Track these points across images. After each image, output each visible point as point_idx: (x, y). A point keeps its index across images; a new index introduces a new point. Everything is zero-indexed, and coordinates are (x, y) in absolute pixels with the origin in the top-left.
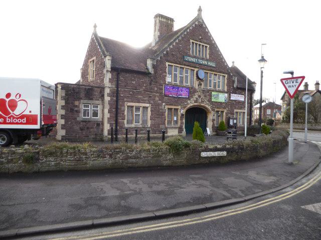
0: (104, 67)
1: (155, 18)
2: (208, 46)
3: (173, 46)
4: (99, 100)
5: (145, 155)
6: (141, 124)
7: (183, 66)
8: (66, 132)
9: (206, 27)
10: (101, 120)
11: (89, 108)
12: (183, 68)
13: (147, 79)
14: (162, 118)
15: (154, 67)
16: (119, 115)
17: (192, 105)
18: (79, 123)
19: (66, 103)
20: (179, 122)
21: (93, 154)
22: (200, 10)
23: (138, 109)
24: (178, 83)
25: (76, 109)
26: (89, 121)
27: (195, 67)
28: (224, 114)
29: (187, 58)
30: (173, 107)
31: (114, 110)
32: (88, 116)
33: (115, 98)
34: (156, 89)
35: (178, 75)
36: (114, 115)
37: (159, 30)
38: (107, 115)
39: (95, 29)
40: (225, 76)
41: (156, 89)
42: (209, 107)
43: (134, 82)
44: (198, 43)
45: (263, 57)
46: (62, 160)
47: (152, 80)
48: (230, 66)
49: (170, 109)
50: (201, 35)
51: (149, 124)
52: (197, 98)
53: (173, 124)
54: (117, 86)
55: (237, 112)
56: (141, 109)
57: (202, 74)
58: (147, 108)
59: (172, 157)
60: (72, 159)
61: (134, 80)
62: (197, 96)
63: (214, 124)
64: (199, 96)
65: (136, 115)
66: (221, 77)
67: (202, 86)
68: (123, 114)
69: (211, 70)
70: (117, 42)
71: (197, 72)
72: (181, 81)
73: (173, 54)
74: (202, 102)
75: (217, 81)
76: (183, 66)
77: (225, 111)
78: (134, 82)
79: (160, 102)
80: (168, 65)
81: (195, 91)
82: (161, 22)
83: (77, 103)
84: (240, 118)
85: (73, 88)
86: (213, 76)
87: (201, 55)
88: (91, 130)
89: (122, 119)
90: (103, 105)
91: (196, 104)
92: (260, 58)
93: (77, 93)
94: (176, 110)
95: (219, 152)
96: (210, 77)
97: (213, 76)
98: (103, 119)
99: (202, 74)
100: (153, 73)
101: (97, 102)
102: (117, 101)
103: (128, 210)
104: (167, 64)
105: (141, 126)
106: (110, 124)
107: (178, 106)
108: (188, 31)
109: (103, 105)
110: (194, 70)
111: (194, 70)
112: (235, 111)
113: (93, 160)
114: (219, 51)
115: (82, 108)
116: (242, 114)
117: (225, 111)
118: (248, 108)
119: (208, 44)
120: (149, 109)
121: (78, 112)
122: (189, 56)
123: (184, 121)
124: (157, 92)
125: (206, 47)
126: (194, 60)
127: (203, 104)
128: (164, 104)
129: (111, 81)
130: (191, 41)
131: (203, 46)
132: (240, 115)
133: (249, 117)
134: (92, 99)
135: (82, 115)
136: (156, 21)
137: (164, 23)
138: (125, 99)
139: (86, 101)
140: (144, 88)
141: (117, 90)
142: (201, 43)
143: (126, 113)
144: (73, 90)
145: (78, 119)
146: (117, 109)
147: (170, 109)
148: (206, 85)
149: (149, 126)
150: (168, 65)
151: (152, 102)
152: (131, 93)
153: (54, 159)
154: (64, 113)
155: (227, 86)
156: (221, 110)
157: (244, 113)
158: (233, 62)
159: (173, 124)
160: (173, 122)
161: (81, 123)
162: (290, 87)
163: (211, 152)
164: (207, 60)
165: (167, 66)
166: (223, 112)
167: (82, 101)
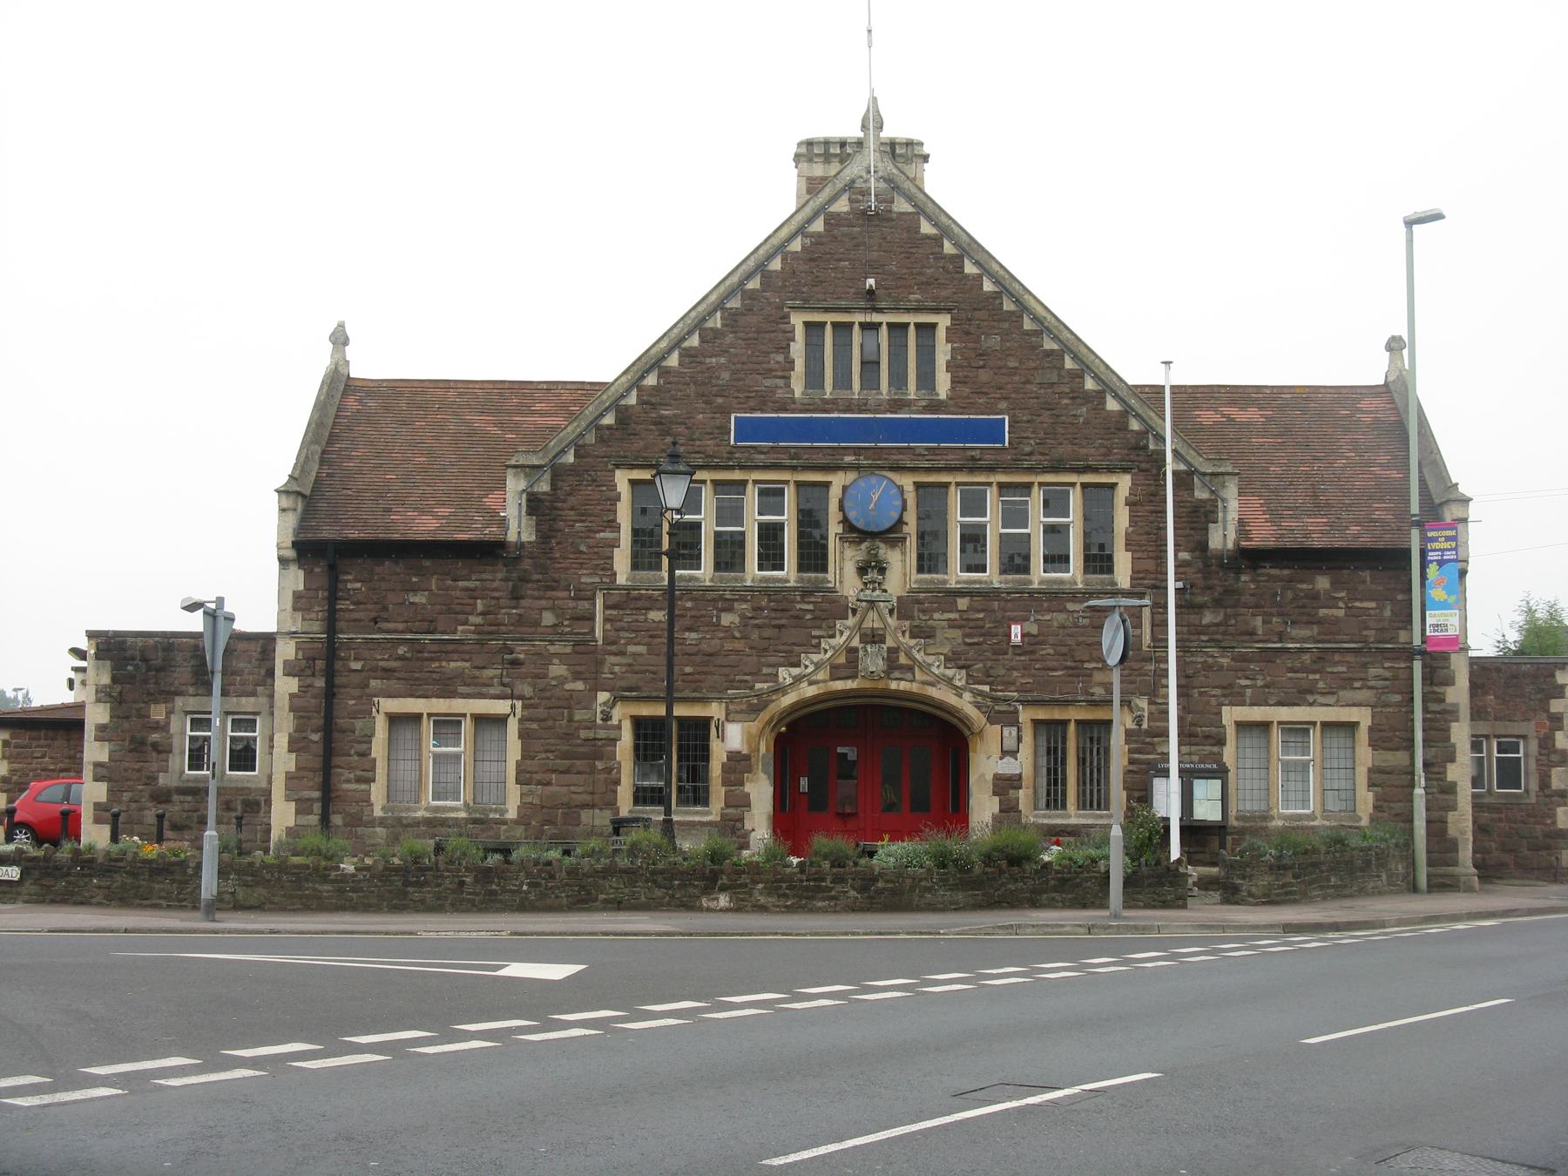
4: (254, 694)
7: (737, 475)
10: (264, 784)
13: (495, 577)
14: (592, 770)
15: (534, 504)
16: (336, 760)
17: (809, 691)
18: (162, 797)
23: (447, 725)
28: (1117, 741)
31: (316, 737)
33: (320, 683)
36: (317, 763)
41: (548, 619)
42: (965, 704)
43: (419, 599)
50: (874, 268)
54: (331, 627)
58: (501, 721)
61: (415, 590)
65: (437, 757)
68: (365, 754)
70: (123, 911)
73: (658, 422)
79: (580, 685)
83: (157, 712)
85: (142, 651)
89: (359, 780)
91: (839, 685)
93: (158, 670)
98: (270, 778)
100: (529, 536)
102: (330, 694)
103: (1049, 404)
104: (622, 479)
105: (463, 815)
107: (704, 700)
110: (933, 326)
111: (933, 326)
112: (1231, 715)
115: (183, 732)
119: (937, 310)
120: (513, 726)
121: (163, 750)
125: (927, 330)
127: (903, 686)
131: (898, 329)
140: (479, 620)
144: (144, 660)
146: (328, 729)
148: (929, 560)
149: (512, 814)
150: (633, 483)
154: (103, 798)
161: (175, 798)
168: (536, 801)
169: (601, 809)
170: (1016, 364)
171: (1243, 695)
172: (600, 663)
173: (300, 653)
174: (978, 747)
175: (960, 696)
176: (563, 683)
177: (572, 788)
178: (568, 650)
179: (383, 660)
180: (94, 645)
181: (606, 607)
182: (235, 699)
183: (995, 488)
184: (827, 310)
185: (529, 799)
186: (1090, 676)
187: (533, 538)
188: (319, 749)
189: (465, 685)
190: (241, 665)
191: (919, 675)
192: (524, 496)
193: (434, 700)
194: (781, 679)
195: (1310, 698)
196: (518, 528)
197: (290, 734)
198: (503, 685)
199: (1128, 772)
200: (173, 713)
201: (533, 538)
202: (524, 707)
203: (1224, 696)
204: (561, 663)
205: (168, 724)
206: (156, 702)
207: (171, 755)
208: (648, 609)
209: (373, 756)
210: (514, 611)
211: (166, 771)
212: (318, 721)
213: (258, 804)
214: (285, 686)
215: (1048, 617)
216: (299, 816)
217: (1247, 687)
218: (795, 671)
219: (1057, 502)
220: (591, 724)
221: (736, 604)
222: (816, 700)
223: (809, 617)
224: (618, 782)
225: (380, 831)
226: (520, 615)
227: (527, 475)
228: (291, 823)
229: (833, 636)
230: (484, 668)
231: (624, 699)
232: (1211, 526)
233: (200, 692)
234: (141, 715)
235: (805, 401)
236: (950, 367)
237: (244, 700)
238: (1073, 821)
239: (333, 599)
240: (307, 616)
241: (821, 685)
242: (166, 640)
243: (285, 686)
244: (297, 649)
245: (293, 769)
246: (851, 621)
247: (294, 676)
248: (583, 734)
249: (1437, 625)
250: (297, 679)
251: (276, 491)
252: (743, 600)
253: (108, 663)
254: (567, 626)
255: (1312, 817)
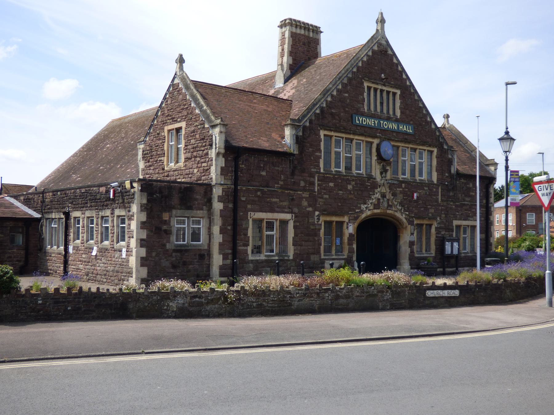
0: (211, 145)
1: (281, 27)
2: (398, 92)
3: (332, 96)
4: (202, 209)
5: (358, 294)
6: (277, 254)
8: (148, 273)
9: (394, 54)
10: (206, 247)
11: (186, 226)
12: (352, 140)
15: (298, 140)
16: (238, 237)
17: (369, 213)
19: (149, 216)
20: (346, 247)
21: (298, 293)
22: (382, 21)
23: (270, 225)
24: (342, 169)
25: (165, 227)
26: (187, 251)
27: (375, 137)
28: (433, 230)
29: (360, 120)
30: (335, 219)
31: (229, 228)
32: (184, 241)
33: (231, 206)
34: (302, 184)
35: (343, 156)
37: (291, 53)
38: (218, 238)
39: (181, 68)
40: (432, 152)
41: (302, 184)
42: (402, 217)
43: (264, 173)
44: (380, 87)
45: (507, 133)
46: (264, 300)
47: (295, 168)
48: (439, 125)
49: (328, 224)
50: (382, 71)
51: (291, 253)
52: (379, 199)
53: (333, 252)
54: (236, 184)
55: (458, 227)
56: (276, 225)
57: (387, 149)
59: (390, 296)
60: (275, 299)
62: (378, 196)
63: (412, 252)
64: (383, 196)
66: (425, 155)
67: (389, 175)
69: (406, 141)
71: (378, 146)
72: (348, 168)
73: (332, 114)
74: (390, 207)
75: (416, 163)
76: (351, 136)
77: (435, 225)
78: (264, 173)
79: (310, 209)
80: (325, 135)
81: (375, 185)
82: (293, 35)
83: (166, 216)
84: (465, 239)
86: (408, 152)
87: (385, 111)
88: (191, 266)
90: (210, 218)
92: (502, 134)
94: (340, 224)
95: (450, 291)
96: (404, 155)
97: (408, 152)
98: (209, 245)
99: (387, 149)
101: (200, 213)
102: (235, 210)
104: (322, 133)
105: (277, 258)
106: (223, 254)
107: (342, 215)
108: (360, 64)
109: (210, 218)
112: (456, 223)
113: (299, 301)
114: (420, 100)
116: (469, 231)
117: (435, 225)
118: (481, 217)
119: (397, 88)
120: (291, 225)
121: (168, 233)
122: (363, 114)
123: (355, 246)
124: (304, 190)
125: (394, 94)
126: (371, 122)
128: (317, 213)
129: (224, 171)
130: (366, 84)
131: (388, 92)
132: (465, 232)
133: (484, 236)
134: (190, 208)
135: (173, 238)
136: (283, 35)
137: (322, 32)
138: (249, 206)
139: (179, 212)
140: (281, 183)
141: (236, 191)
142: (384, 88)
143: (250, 233)
145: (168, 246)
147: (328, 224)
148: (395, 172)
149: (291, 258)
150: (325, 135)
151: (296, 210)
152: (259, 193)
153: (256, 299)
155: (437, 171)
156: (425, 222)
157: (474, 227)
158: (447, 117)
159: (333, 252)
160: (334, 248)
161: (174, 254)
162: (543, 195)
163: (439, 291)
164: (397, 121)
165: (322, 137)
166: (430, 226)
167: (174, 212)
168: (299, 252)
169: (316, 255)
170: (414, 110)
171: (457, 217)
172: (316, 201)
173: (224, 193)
174: (404, 232)
175: (402, 215)
176: (306, 208)
177: (309, 247)
178: (308, 196)
179: (252, 197)
180: (140, 185)
181: (318, 180)
182: (195, 211)
183: (409, 149)
184: (373, 83)
185: (296, 252)
186: (429, 210)
187: (297, 153)
188: (231, 233)
189: (277, 208)
190: (198, 197)
191: (394, 209)
192: (295, 136)
193: (268, 213)
194: (362, 209)
195: (469, 218)
196: (294, 149)
197: (220, 227)
198: (289, 208)
199: (436, 240)
200: (172, 217)
201: (297, 153)
202: (295, 217)
203: (454, 217)
204: (306, 201)
205: (170, 221)
206: (165, 211)
207: (171, 235)
208: (330, 182)
209: (248, 235)
210: (292, 180)
211: (169, 242)
212: (230, 221)
213: (204, 255)
214: (218, 206)
215: (421, 191)
216: (224, 261)
217: (458, 215)
218: (366, 206)
219: (358, 149)
220: (314, 224)
221: (351, 182)
222: (369, 216)
223: (369, 187)
224: (321, 245)
225: (251, 265)
226: (294, 182)
227: (296, 129)
228: (221, 264)
229: (374, 195)
230: (284, 201)
231: (323, 214)
232: (452, 166)
233: (182, 208)
234: (160, 217)
235: (368, 113)
236: (400, 108)
237: (198, 212)
238: (425, 255)
239: (236, 172)
240: (226, 178)
241: (372, 211)
242: (169, 184)
243: (218, 206)
244: (223, 191)
245: (222, 241)
246: (379, 190)
247: (222, 202)
248: (312, 227)
249: (513, 199)
250: (222, 203)
251: (498, 139)
252: (353, 180)
253: (146, 194)
254: (308, 187)
255: (467, 253)
